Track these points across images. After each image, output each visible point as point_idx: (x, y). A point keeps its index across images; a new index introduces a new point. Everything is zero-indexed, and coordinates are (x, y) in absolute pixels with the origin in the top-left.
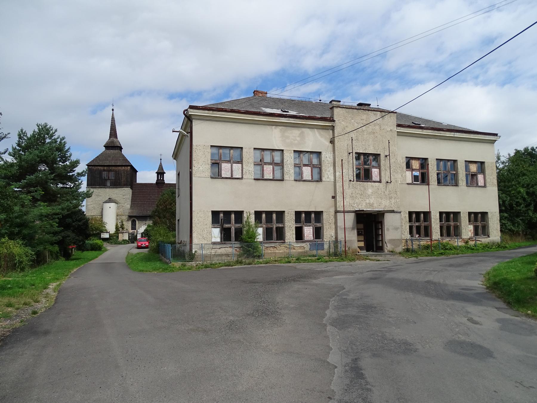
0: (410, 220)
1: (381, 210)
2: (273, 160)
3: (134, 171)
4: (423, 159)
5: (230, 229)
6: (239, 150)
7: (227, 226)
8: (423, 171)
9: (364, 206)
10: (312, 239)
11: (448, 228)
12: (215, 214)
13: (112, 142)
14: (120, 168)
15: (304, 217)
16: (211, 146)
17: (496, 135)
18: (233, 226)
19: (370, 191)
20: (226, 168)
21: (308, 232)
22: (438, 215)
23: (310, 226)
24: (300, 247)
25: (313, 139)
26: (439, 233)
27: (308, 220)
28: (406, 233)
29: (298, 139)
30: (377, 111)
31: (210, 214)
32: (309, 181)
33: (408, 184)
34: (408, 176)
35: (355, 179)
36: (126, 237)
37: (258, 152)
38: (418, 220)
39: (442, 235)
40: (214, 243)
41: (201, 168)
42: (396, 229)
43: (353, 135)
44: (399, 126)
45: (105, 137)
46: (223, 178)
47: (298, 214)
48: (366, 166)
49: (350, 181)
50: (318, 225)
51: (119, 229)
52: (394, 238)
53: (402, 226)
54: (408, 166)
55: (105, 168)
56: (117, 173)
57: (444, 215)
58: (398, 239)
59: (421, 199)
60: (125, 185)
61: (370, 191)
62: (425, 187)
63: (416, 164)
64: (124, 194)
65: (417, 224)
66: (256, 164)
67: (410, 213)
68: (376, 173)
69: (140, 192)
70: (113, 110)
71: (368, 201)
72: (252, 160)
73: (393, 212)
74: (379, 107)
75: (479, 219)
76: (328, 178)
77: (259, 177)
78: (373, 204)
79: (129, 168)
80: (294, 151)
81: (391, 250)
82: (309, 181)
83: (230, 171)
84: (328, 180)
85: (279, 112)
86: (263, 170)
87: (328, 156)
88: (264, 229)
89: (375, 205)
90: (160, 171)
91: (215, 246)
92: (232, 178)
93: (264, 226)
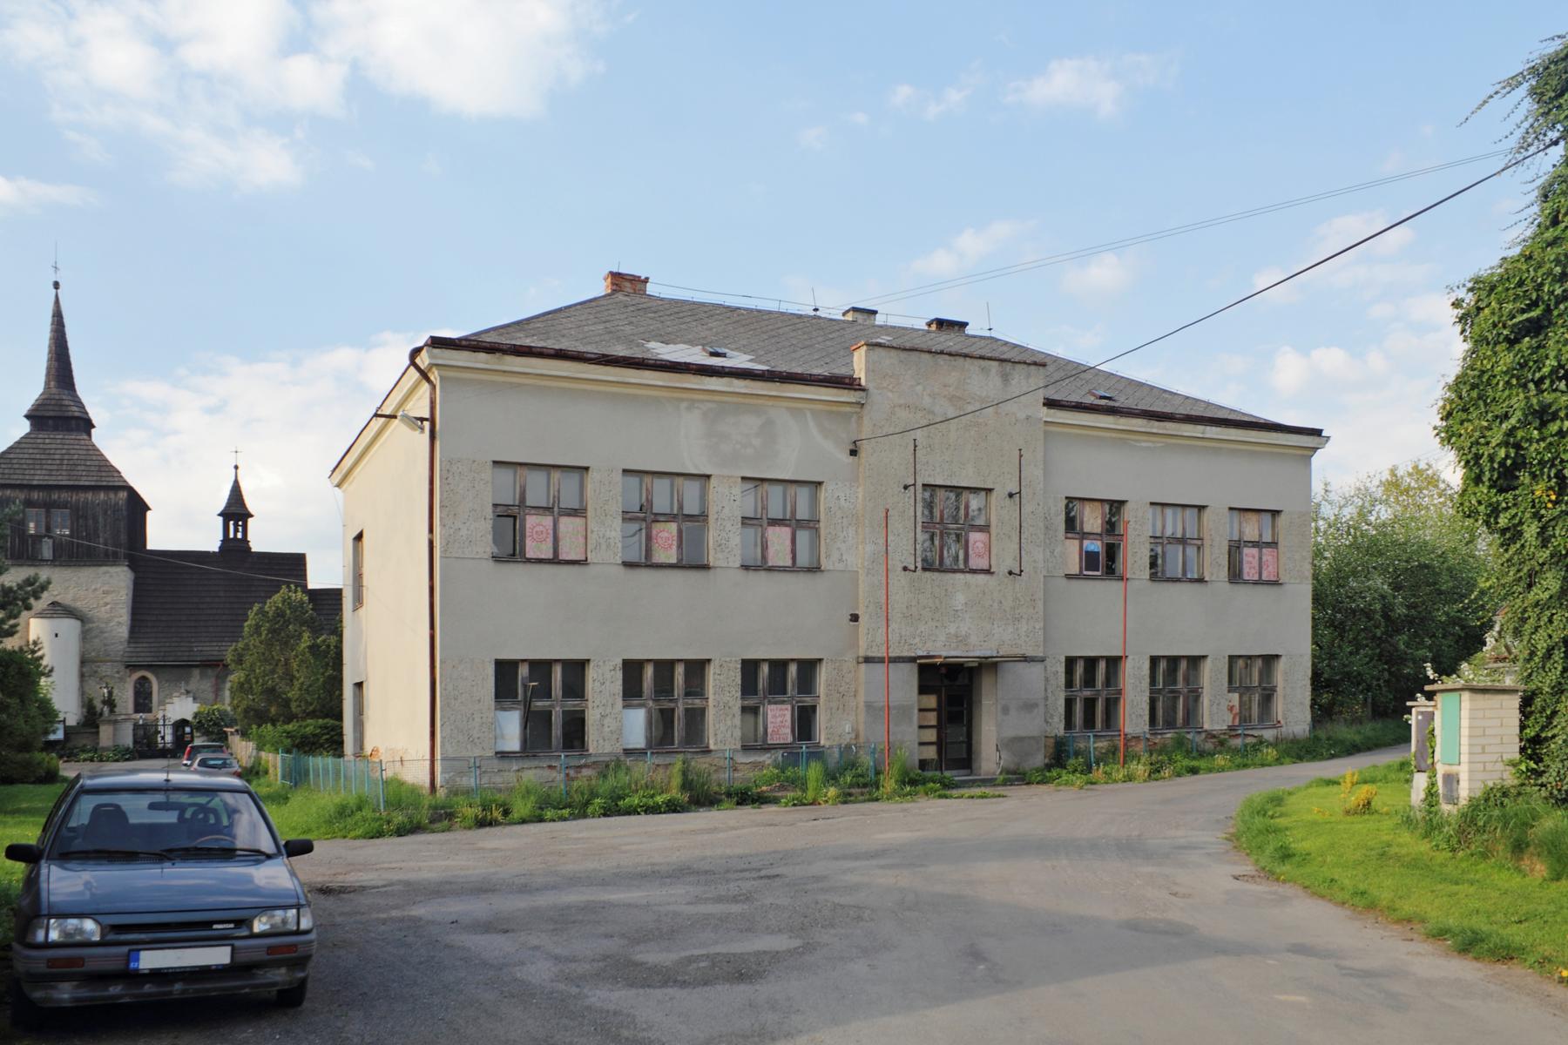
0: (1069, 684)
1: (988, 654)
2: (681, 507)
3: (137, 507)
4: (1112, 503)
5: (547, 715)
6: (576, 476)
7: (539, 704)
8: (1111, 540)
9: (942, 648)
10: (790, 739)
11: (1090, 704)
12: (505, 670)
13: (59, 404)
14: (89, 496)
15: (767, 679)
16: (495, 463)
17: (1317, 433)
18: (558, 707)
19: (960, 599)
20: (537, 526)
21: (779, 719)
22: (1147, 665)
23: (783, 702)
24: (755, 765)
25: (796, 439)
26: (1147, 718)
27: (777, 687)
28: (1056, 719)
29: (756, 442)
30: (990, 359)
31: (490, 670)
32: (783, 569)
33: (1069, 577)
34: (1071, 554)
35: (919, 565)
36: (127, 740)
37: (634, 481)
38: (1089, 681)
39: (1069, 724)
40: (503, 755)
41: (464, 532)
42: (1029, 706)
43: (919, 434)
44: (1050, 404)
45: (32, 386)
46: (529, 561)
47: (750, 668)
48: (946, 527)
49: (905, 569)
50: (808, 700)
51: (91, 720)
52: (1022, 733)
53: (1046, 699)
54: (1071, 524)
55: (35, 495)
56: (79, 515)
57: (1163, 665)
58: (1033, 738)
59: (1107, 620)
60: (108, 559)
61: (960, 599)
62: (1114, 586)
63: (1092, 520)
64: (107, 592)
65: (1087, 693)
66: (627, 517)
67: (1070, 662)
68: (980, 545)
69: (165, 582)
70: (56, 285)
71: (952, 630)
72: (616, 508)
73: (1025, 659)
74: (993, 334)
75: (1254, 674)
76: (840, 560)
77: (636, 555)
78: (967, 636)
79: (123, 495)
80: (744, 478)
81: (1012, 767)
82: (783, 569)
83: (550, 540)
84: (840, 566)
85: (697, 356)
86: (649, 538)
87: (842, 495)
88: (649, 713)
89: (973, 640)
90: (233, 510)
91: (505, 764)
92: (555, 561)
93: (651, 703)
